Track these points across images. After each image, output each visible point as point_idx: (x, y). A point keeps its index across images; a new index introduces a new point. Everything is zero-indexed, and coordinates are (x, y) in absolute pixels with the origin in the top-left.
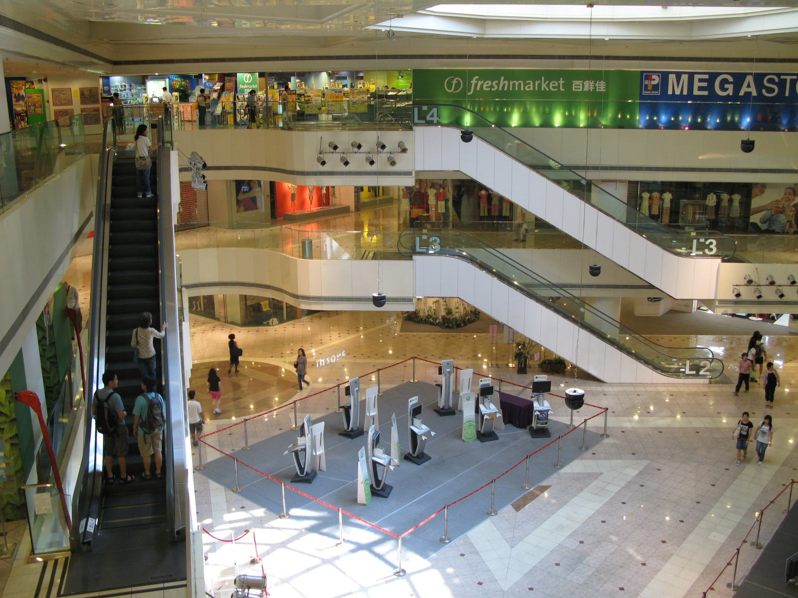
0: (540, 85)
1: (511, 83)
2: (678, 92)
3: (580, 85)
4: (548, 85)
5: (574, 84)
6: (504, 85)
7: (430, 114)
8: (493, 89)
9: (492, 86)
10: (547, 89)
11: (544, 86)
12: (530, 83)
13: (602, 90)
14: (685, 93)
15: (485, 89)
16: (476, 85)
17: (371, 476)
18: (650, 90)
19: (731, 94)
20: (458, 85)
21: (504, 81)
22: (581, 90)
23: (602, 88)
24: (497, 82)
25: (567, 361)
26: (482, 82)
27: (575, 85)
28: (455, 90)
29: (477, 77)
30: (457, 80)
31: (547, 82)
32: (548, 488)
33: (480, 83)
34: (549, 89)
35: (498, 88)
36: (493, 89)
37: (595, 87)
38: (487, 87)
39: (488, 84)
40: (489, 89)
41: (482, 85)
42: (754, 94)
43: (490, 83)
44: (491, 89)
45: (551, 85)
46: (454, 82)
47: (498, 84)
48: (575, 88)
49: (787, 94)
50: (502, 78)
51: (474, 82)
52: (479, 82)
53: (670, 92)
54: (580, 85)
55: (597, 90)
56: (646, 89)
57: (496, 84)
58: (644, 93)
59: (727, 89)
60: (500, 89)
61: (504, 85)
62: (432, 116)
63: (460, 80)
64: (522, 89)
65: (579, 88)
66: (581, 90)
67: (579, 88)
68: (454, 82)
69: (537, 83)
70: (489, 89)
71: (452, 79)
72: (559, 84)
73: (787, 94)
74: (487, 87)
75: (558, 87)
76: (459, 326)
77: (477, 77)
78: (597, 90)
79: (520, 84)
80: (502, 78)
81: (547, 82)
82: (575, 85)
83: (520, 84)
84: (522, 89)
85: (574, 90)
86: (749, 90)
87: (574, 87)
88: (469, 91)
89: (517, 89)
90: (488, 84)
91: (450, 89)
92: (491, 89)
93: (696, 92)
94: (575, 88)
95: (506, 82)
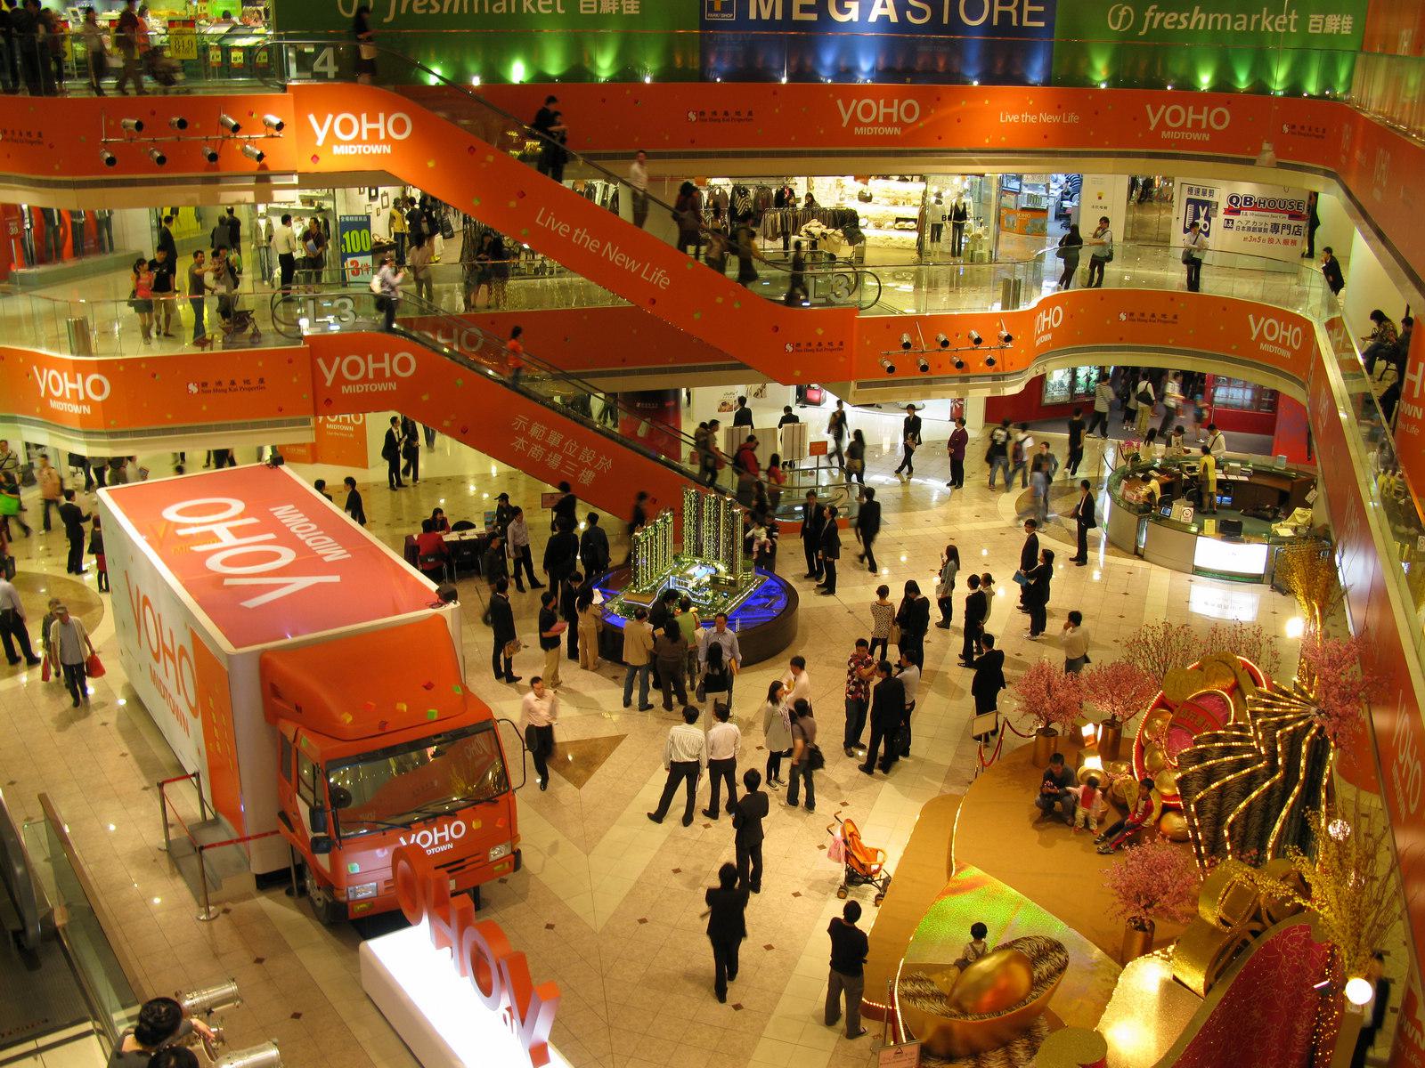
0: (1258, 23)
1: (1211, 17)
2: (766, 15)
3: (1318, 23)
4: (1272, 23)
5: (1311, 21)
6: (1199, 20)
7: (320, 59)
8: (431, 12)
9: (1178, 22)
10: (534, 11)
11: (1265, 23)
12: (1242, 19)
13: (633, 12)
14: (778, 16)
15: (416, 10)
16: (1152, 19)
17: (79, 964)
18: (716, 12)
19: (856, 19)
20: (1126, 19)
21: (1199, 12)
22: (595, 12)
23: (633, 7)
24: (1188, 15)
25: (1218, 539)
26: (1163, 14)
27: (1314, 23)
28: (1121, 28)
29: (1155, 7)
30: (1126, 10)
31: (1272, 17)
32: (621, 740)
33: (1158, 16)
34: (1274, 29)
35: (1189, 25)
36: (431, 12)
37: (621, 7)
38: (1170, 24)
39: (1172, 17)
40: (424, 11)
41: (1162, 20)
42: (894, 19)
43: (1176, 16)
44: (428, 11)
45: (1277, 22)
46: (1122, 13)
47: (1189, 19)
48: (1313, 28)
49: (946, 21)
50: (1197, 8)
51: (1149, 14)
52: (1158, 14)
53: (753, 16)
54: (1318, 23)
55: (625, 12)
56: (711, 10)
57: (1186, 18)
58: (709, 17)
59: (849, 10)
60: (1192, 27)
61: (1199, 20)
62: (324, 63)
63: (1130, 9)
64: (487, 11)
65: (592, 9)
66: (595, 12)
67: (592, 9)
68: (1122, 13)
69: (1254, 18)
70: (424, 11)
71: (1119, 9)
72: (1289, 21)
73: (946, 21)
74: (1170, 24)
75: (1287, 26)
76: (1327, 586)
77: (1155, 7)
78: (625, 12)
79: (1225, 21)
80: (1197, 8)
81: (1272, 17)
82: (1314, 23)
83: (1225, 21)
84: (487, 11)
85: (582, 11)
86: (883, 12)
87: (1311, 25)
88: (387, 16)
89: (476, 11)
90: (1172, 17)
91: (1115, 25)
92: (428, 11)
93: (797, 15)
94: (1313, 28)
95: (1203, 16)
